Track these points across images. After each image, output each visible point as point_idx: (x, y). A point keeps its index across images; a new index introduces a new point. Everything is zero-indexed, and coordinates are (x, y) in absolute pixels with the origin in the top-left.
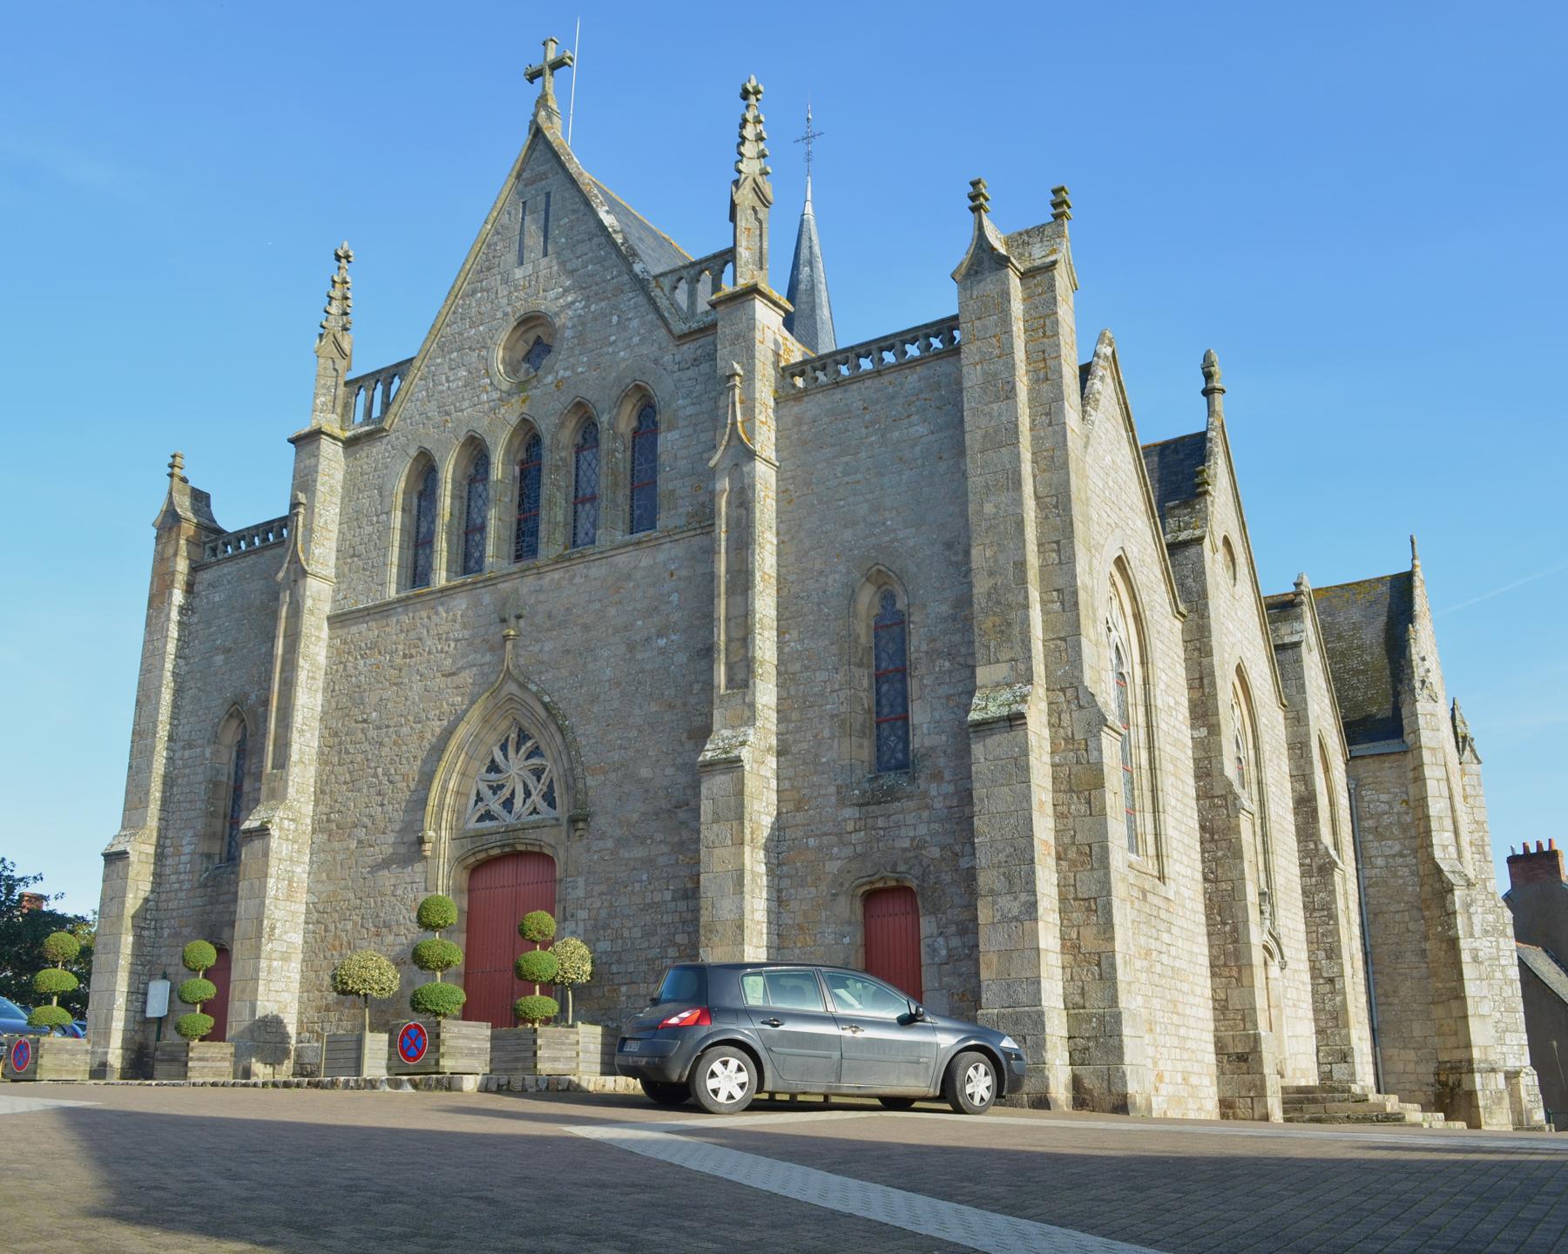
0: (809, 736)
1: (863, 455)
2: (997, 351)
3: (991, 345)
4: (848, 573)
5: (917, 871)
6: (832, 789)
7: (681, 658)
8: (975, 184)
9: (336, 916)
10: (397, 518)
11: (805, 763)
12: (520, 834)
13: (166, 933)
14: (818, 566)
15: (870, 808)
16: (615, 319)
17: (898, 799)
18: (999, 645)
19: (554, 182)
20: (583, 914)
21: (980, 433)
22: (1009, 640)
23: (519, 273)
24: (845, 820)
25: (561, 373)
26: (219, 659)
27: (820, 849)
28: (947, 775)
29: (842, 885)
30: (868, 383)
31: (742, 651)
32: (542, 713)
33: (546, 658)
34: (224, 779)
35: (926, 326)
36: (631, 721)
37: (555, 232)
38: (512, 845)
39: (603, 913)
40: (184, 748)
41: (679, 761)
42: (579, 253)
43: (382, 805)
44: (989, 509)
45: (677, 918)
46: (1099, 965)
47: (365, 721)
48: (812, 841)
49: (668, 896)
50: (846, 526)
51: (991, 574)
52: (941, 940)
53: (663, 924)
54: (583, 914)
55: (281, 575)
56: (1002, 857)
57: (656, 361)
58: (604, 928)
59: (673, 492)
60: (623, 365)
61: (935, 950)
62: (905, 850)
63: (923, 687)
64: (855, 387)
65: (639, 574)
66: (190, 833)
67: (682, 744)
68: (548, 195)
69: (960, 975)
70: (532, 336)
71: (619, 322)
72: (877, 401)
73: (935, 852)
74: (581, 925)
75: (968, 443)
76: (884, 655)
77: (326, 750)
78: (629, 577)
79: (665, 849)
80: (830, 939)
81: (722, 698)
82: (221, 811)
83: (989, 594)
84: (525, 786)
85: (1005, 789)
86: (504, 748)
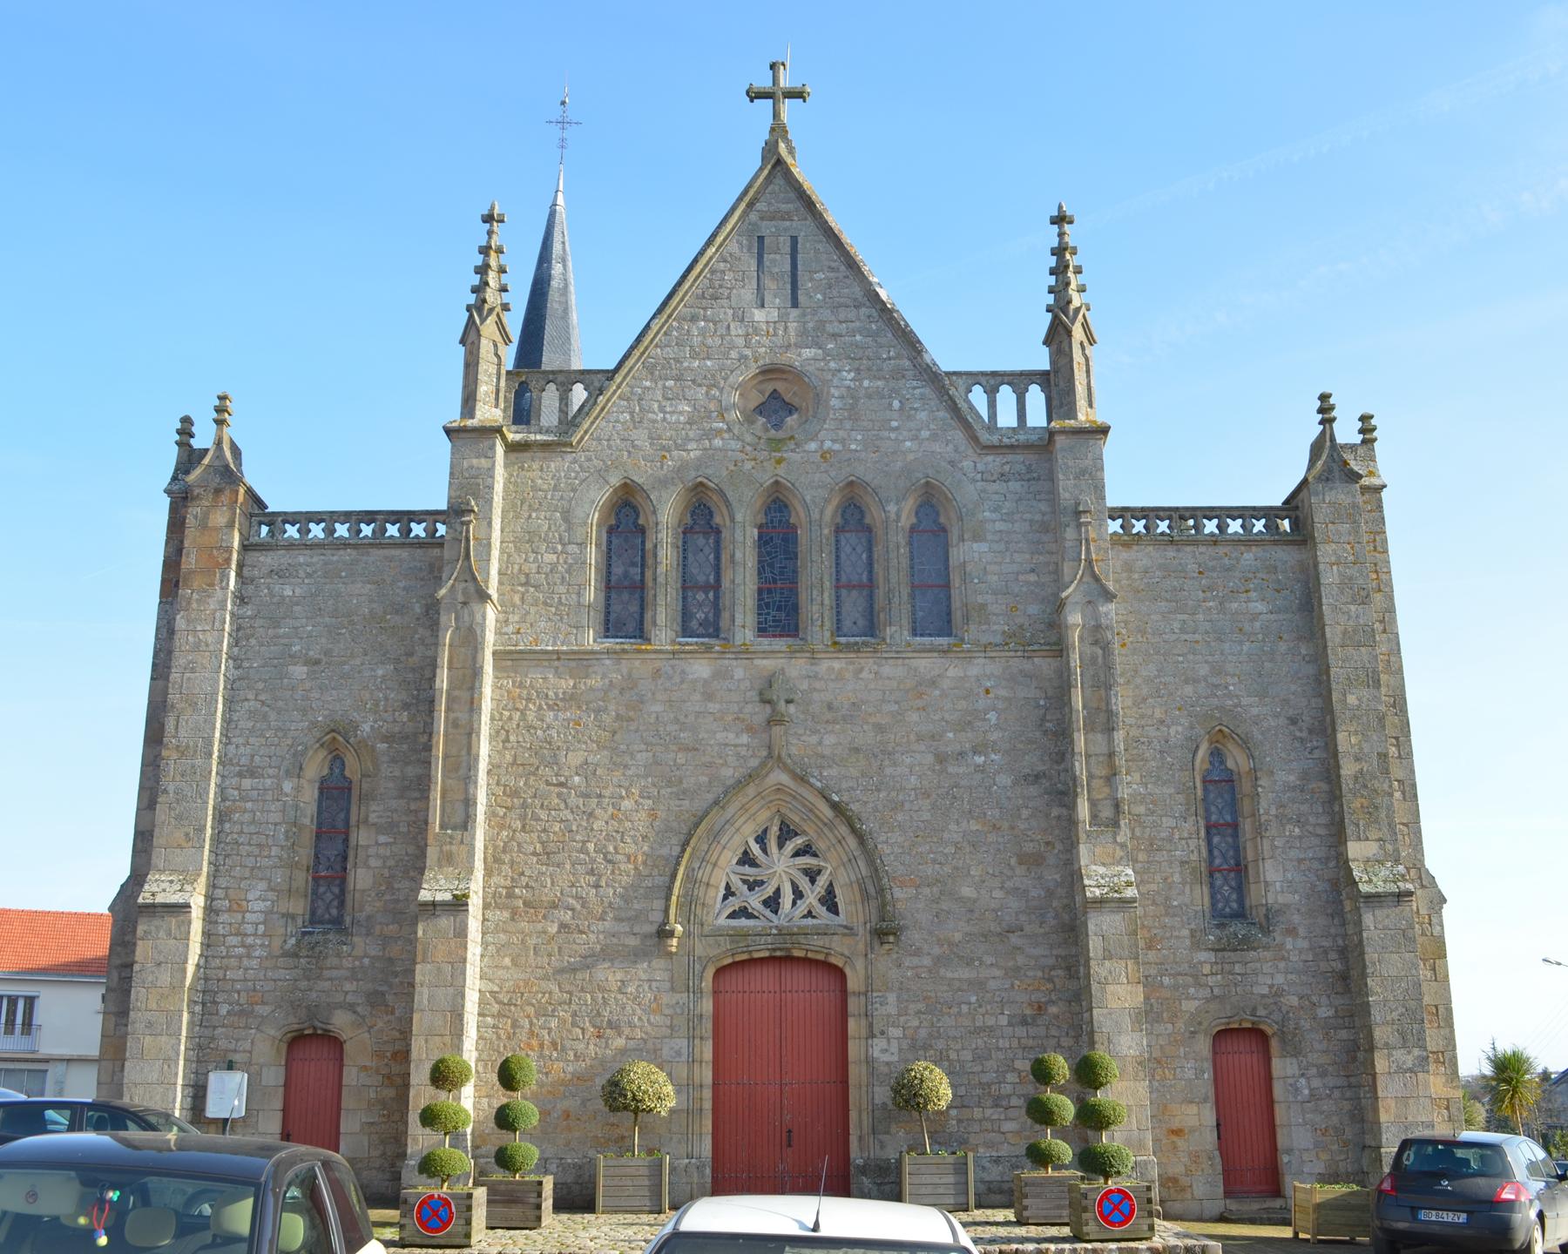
0: (1158, 878)
1: (1201, 617)
2: (1351, 558)
3: (1345, 550)
4: (1192, 728)
5: (1277, 1016)
6: (1186, 932)
7: (1004, 780)
8: (222, 398)
9: (530, 1010)
10: (592, 555)
11: (1154, 903)
12: (802, 939)
13: (224, 1009)
14: (1158, 713)
15: (1227, 954)
16: (896, 404)
17: (1254, 949)
18: (1367, 825)
19: (804, 228)
20: (895, 1032)
21: (1339, 629)
22: (1376, 821)
23: (759, 315)
24: (1201, 963)
25: (828, 444)
26: (299, 671)
27: (1175, 987)
28: (1302, 931)
29: (1200, 1023)
30: (1202, 549)
31: (1107, 790)
32: (828, 812)
33: (827, 752)
34: (307, 821)
35: (1254, 508)
36: (946, 835)
37: (806, 284)
38: (788, 949)
39: (923, 1033)
40: (240, 775)
41: (1009, 884)
42: (842, 317)
43: (597, 886)
44: (1352, 700)
45: (1015, 1043)
46: (1447, 1108)
47: (561, 785)
48: (1166, 980)
49: (1004, 1021)
50: (1186, 682)
51: (1357, 759)
52: (1303, 1081)
53: (999, 1049)
54: (895, 1032)
55: (443, 592)
56: (1395, 1015)
57: (952, 463)
58: (926, 1047)
59: (983, 607)
60: (911, 457)
61: (1297, 1089)
62: (1263, 996)
63: (1273, 848)
64: (1189, 549)
65: (946, 684)
66: (262, 885)
67: (1012, 869)
68: (794, 240)
69: (1322, 1113)
70: (769, 388)
71: (901, 409)
72: (1214, 569)
73: (1294, 1001)
74: (894, 1043)
75: (1328, 635)
76: (1213, 809)
77: (501, 812)
78: (933, 683)
79: (998, 973)
80: (1190, 1074)
81: (1088, 834)
82: (305, 862)
83: (1356, 778)
84: (793, 884)
85: (1395, 956)
86: (761, 840)
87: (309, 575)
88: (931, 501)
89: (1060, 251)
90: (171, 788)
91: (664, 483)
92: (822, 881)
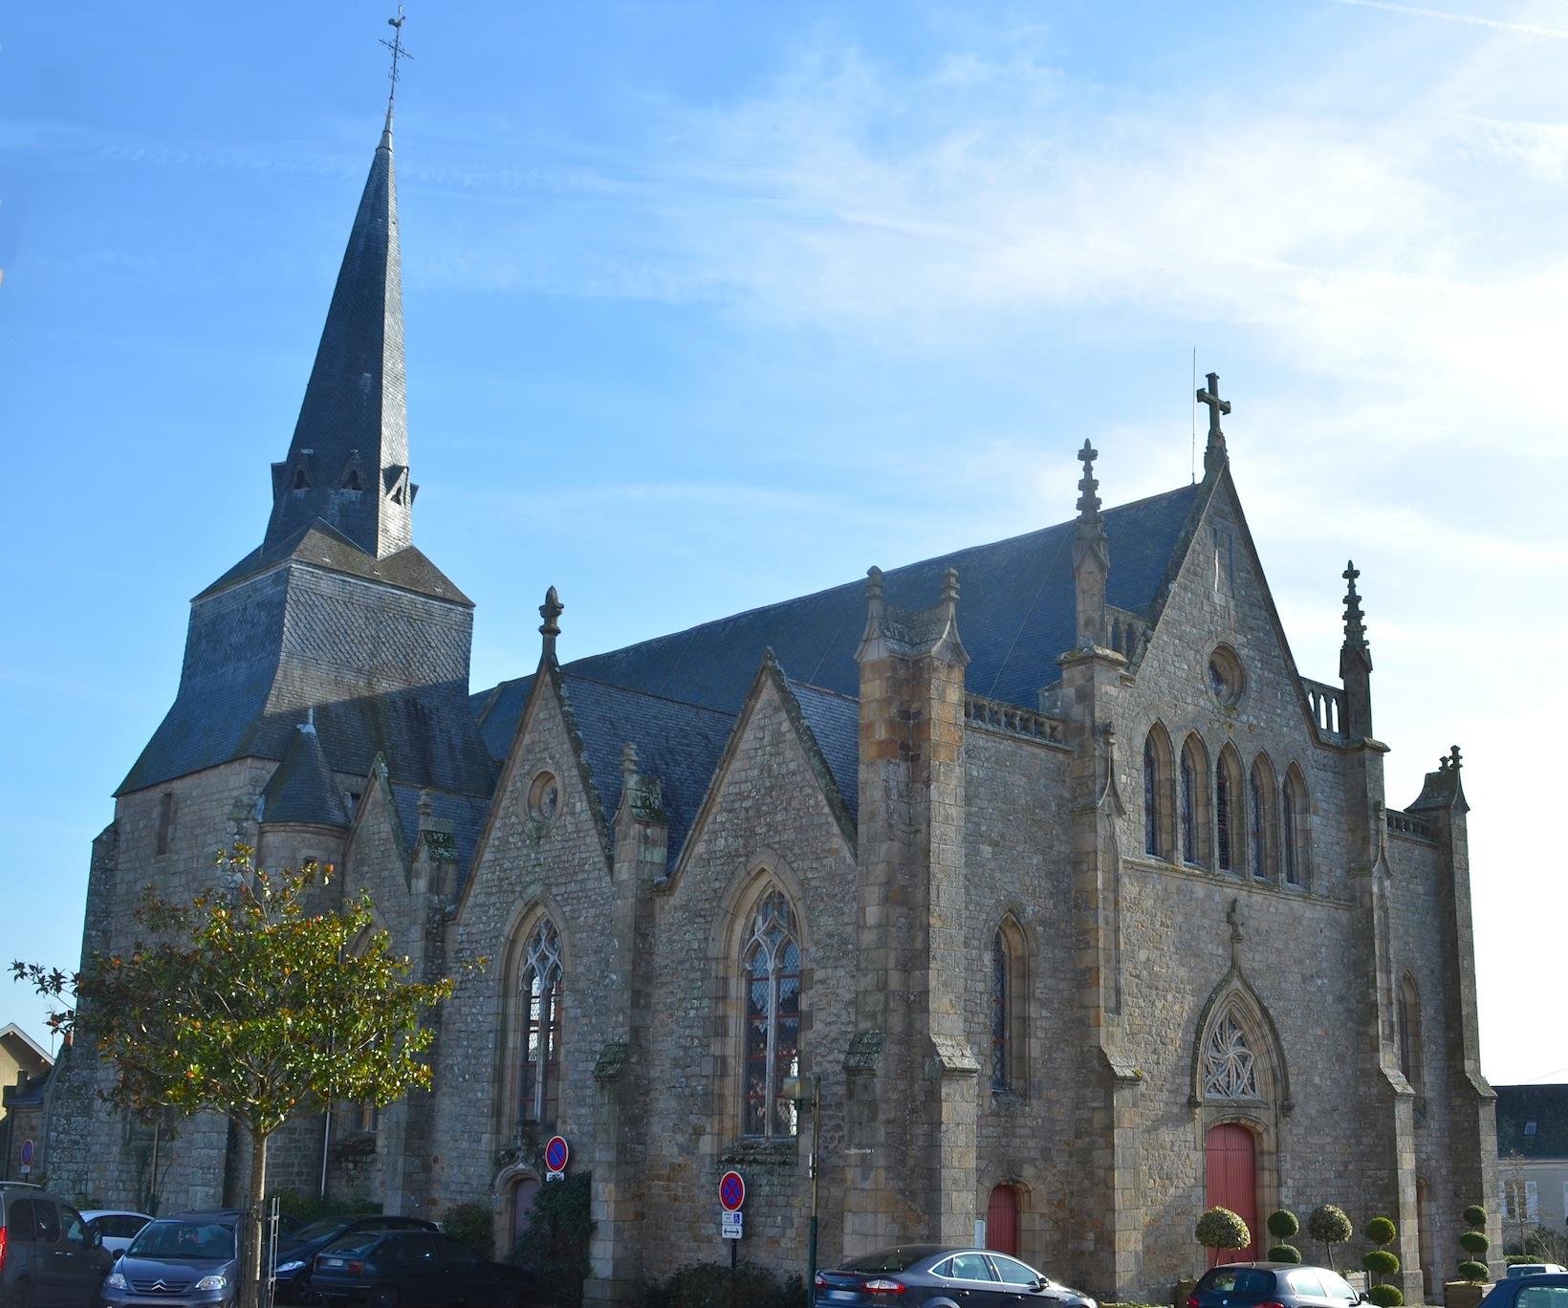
7: (1330, 998)
87: (987, 760)
88: (1294, 773)
89: (1352, 600)
90: (938, 956)
91: (1179, 729)
92: (1249, 1064)
